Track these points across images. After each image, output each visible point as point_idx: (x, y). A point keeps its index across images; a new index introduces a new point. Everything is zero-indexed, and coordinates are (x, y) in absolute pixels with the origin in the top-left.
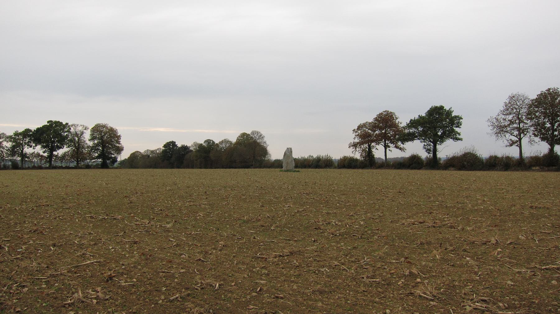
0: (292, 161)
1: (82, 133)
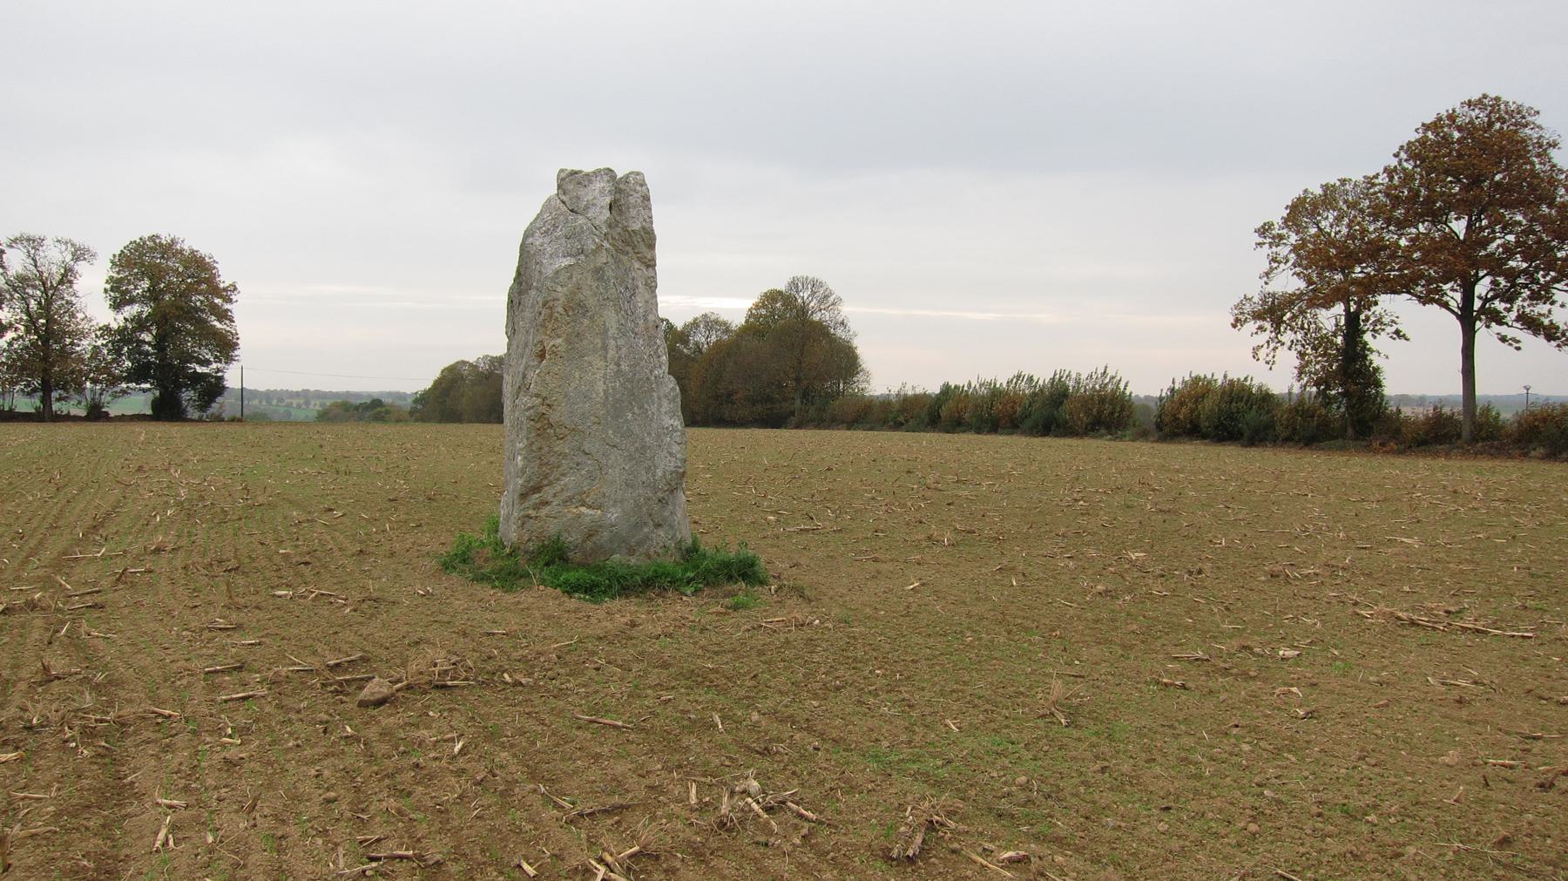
0: (634, 392)
1: (67, 276)
